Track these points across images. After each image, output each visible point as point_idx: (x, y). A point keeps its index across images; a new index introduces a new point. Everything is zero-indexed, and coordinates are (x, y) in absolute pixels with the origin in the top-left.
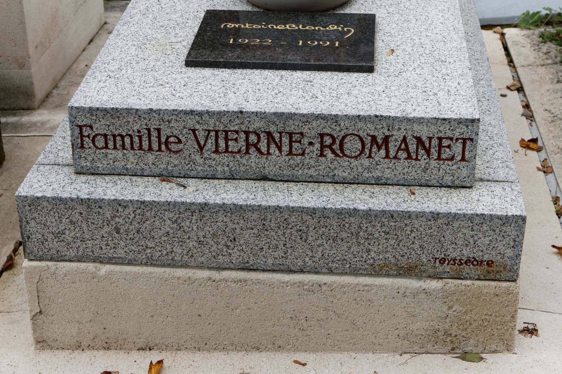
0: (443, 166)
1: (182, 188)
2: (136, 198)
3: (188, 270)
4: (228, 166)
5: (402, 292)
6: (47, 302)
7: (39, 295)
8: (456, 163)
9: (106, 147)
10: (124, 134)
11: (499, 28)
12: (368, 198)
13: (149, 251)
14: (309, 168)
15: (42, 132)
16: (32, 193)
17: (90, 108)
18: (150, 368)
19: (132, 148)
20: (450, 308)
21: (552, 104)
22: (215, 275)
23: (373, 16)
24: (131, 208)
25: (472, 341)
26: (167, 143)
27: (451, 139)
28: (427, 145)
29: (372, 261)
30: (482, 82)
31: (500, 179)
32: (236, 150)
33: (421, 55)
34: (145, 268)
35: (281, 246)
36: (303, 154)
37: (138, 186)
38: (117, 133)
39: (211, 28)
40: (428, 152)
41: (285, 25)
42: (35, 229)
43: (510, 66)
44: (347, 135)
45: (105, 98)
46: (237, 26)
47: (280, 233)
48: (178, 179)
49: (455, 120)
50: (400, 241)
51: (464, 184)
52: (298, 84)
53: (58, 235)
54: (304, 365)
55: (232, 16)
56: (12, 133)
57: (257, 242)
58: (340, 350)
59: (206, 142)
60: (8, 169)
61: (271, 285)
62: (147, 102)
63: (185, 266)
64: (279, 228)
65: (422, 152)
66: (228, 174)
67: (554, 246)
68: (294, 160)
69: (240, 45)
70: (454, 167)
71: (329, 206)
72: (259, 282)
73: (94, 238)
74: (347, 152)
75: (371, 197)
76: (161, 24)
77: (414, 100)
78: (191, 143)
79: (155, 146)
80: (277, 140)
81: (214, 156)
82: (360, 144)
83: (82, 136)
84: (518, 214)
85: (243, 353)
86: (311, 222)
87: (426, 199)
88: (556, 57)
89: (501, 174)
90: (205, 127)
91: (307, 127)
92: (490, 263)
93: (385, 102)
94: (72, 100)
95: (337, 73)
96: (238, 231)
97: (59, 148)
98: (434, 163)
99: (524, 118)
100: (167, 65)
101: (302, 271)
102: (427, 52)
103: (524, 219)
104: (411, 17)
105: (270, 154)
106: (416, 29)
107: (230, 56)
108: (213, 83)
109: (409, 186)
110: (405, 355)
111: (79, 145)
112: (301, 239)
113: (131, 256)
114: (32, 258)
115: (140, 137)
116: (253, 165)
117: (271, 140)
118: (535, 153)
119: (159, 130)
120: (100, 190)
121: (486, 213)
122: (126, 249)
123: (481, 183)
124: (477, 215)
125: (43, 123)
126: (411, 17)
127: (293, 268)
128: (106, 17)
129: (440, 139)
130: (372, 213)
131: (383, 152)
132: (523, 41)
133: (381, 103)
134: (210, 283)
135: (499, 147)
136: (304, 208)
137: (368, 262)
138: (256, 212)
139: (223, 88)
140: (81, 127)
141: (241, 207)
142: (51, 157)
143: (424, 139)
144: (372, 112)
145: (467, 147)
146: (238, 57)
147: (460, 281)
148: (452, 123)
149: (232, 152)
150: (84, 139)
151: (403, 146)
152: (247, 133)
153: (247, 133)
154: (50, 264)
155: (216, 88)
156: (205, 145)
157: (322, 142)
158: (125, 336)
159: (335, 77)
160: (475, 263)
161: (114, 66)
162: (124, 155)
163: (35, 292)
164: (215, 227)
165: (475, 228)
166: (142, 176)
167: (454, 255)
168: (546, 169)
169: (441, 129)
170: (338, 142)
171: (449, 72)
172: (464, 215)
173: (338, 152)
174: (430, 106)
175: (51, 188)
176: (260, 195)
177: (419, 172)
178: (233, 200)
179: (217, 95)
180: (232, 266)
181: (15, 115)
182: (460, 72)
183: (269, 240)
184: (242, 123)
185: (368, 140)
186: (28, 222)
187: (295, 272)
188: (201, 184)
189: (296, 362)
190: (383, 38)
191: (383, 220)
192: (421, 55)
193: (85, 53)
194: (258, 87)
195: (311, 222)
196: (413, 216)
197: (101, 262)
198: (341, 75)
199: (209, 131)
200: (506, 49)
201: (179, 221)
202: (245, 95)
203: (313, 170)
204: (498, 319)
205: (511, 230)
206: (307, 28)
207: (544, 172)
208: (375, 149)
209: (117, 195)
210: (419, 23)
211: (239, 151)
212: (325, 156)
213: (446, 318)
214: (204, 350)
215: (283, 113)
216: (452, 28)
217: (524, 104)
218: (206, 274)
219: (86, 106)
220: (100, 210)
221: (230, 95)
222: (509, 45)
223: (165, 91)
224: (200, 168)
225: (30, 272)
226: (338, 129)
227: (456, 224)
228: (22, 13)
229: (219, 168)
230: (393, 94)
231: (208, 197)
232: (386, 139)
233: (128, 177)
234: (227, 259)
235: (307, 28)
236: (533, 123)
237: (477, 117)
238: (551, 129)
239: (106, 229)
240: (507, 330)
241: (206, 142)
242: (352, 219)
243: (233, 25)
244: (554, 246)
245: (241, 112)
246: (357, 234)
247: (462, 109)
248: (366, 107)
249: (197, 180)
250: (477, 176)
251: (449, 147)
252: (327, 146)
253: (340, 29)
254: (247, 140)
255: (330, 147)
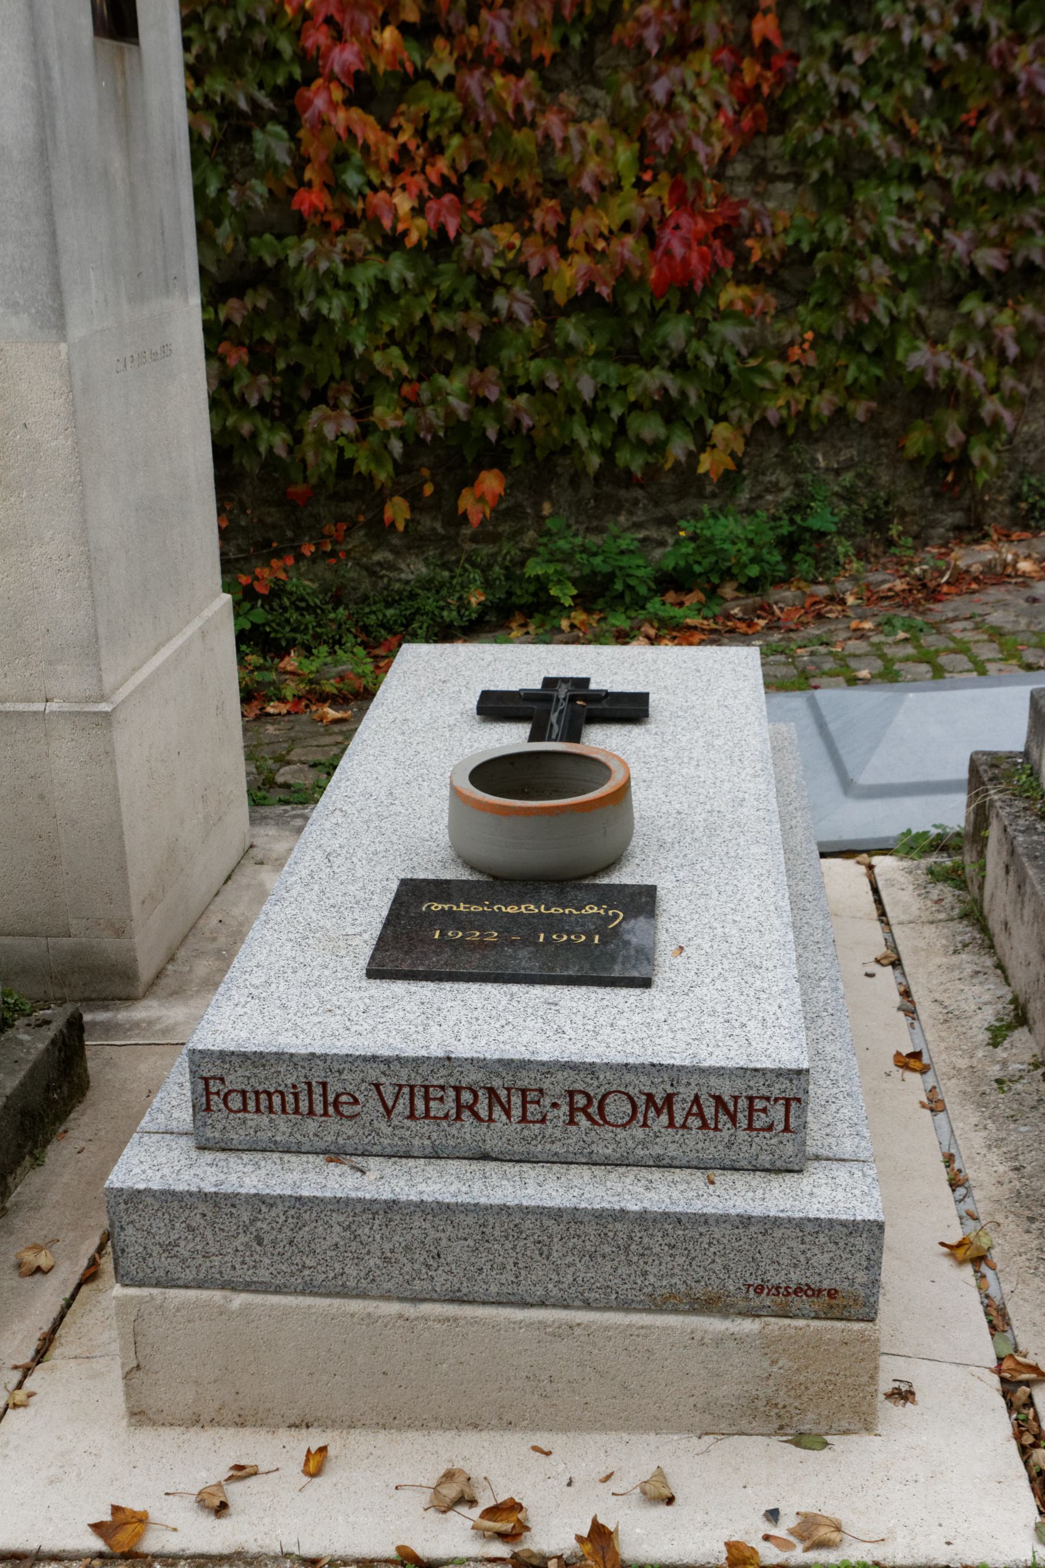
0: (757, 1140)
1: (359, 1174)
2: (288, 1192)
3: (366, 1302)
4: (429, 1138)
5: (698, 1337)
6: (148, 1350)
7: (135, 1339)
8: (776, 1135)
9: (245, 1109)
10: (272, 1090)
11: (865, 855)
12: (642, 1190)
13: (306, 1272)
14: (553, 1142)
15: (148, 1038)
16: (130, 1184)
17: (221, 1052)
18: (307, 1460)
19: (284, 1111)
20: (774, 1362)
21: (945, 991)
22: (410, 1310)
23: (654, 888)
24: (280, 1207)
25: (810, 1416)
26: (336, 1104)
27: (768, 1099)
28: (732, 1108)
29: (650, 1288)
30: (823, 983)
31: (846, 1157)
32: (441, 1114)
33: (724, 956)
34: (301, 1298)
35: (510, 1266)
36: (543, 1121)
37: (291, 1171)
38: (260, 1088)
39: (407, 912)
40: (733, 1118)
41: (519, 904)
42: (134, 1239)
43: (882, 922)
44: (610, 1093)
45: (244, 1035)
46: (446, 907)
47: (508, 1245)
48: (353, 1158)
49: (772, 1071)
50: (693, 1259)
51: (790, 1166)
52: (536, 1008)
53: (169, 1248)
54: (548, 1454)
55: (440, 889)
56: (101, 1039)
57: (473, 1260)
58: (605, 1428)
59: (395, 1102)
60: (93, 1104)
61: (495, 1326)
62: (308, 1041)
63: (363, 1295)
64: (507, 1238)
65: (723, 1118)
66: (430, 1150)
67: (942, 1244)
68: (529, 1129)
69: (451, 942)
70: (774, 1141)
71: (583, 1205)
72: (475, 1321)
73: (224, 1252)
74: (610, 1118)
75: (647, 1189)
76: (332, 901)
77: (710, 1036)
78: (374, 1105)
79: (319, 1108)
80: (504, 1100)
81: (408, 1123)
82: (629, 1106)
83: (208, 1093)
84: (872, 1218)
85: (454, 1432)
86: (556, 1228)
87: (732, 1192)
88: (953, 908)
89: (848, 1147)
90: (395, 1081)
91: (548, 1081)
92: (832, 1293)
93: (667, 1040)
94: (195, 1038)
95: (595, 988)
96: (444, 1243)
97: (174, 1103)
98: (742, 1135)
99: (901, 1014)
100: (339, 975)
101: (542, 1304)
102: (734, 950)
103: (881, 1226)
104: (712, 887)
105: (493, 1121)
106: (718, 910)
107: (435, 962)
108: (408, 1008)
109: (706, 1168)
110: (706, 1438)
111: (204, 1107)
112: (541, 1254)
113: (280, 1280)
114: (127, 1282)
115: (296, 1096)
116: (468, 1136)
117: (494, 1100)
118: (917, 1075)
119: (324, 1085)
120: (233, 1178)
121: (823, 1216)
122: (272, 1269)
123: (816, 1164)
124: (809, 1220)
125: (150, 1023)
126: (712, 887)
127: (529, 1300)
128: (253, 836)
129: (751, 1099)
130: (648, 1216)
131: (664, 1118)
132: (902, 880)
133: (660, 1041)
134: (400, 1322)
135: (836, 1117)
136: (544, 1208)
137: (645, 1290)
138: (471, 1215)
139: (423, 1017)
140: (206, 1080)
141: (448, 1205)
142: (161, 1118)
143: (726, 1098)
144: (647, 1059)
145: (792, 1111)
146: (446, 964)
147: (787, 1321)
148: (768, 1075)
149: (435, 1118)
150: (212, 1097)
151: (695, 1109)
152: (458, 1090)
153: (458, 1090)
154: (155, 1291)
155: (411, 1017)
156: (394, 1107)
157: (571, 1103)
158: (268, 1405)
159: (593, 996)
160: (810, 1292)
161: (258, 978)
162: (271, 1121)
163: (131, 1335)
164: (409, 1237)
165: (807, 1239)
166: (299, 1152)
167: (776, 1281)
168: (935, 1105)
169: (751, 1084)
170: (596, 1103)
171: (766, 985)
172: (790, 1220)
173: (597, 1118)
174: (735, 1046)
175: (159, 1174)
176: (478, 1185)
177: (720, 1148)
178: (437, 1195)
179: (413, 1029)
180: (435, 1296)
181: (106, 1008)
182: (782, 986)
183: (491, 1257)
184: (451, 1075)
185: (641, 1101)
186: (122, 1228)
187: (532, 1305)
188: (388, 1167)
189: (536, 1449)
190: (668, 925)
191: (666, 1226)
192: (724, 956)
193: (218, 899)
194: (476, 1013)
195: (555, 1229)
196: (712, 1221)
197: (233, 1289)
198: (601, 992)
199: (401, 1086)
200: (875, 890)
201: (354, 1227)
202: (456, 1029)
203: (558, 1144)
204: (849, 1381)
205: (861, 1242)
206: (552, 911)
207: (932, 1110)
208: (652, 1114)
209: (260, 1186)
210: (723, 898)
211: (446, 1117)
212: (577, 1124)
213: (768, 1378)
214: (391, 1428)
215: (512, 1061)
216: (772, 908)
217: (902, 989)
218: (392, 1308)
219: (215, 1048)
220: (234, 1210)
221: (433, 1029)
222: (881, 885)
223: (334, 1022)
224: (386, 1142)
225: (123, 1304)
226: (596, 1083)
227: (778, 1233)
228: (123, 852)
229: (416, 1142)
230: (679, 1026)
231: (398, 1190)
232: (669, 1099)
233: (276, 1155)
234: (427, 1285)
235: (552, 911)
236: (916, 1024)
237: (805, 1065)
238: (943, 1034)
239: (242, 1238)
240: (864, 1398)
241: (395, 1102)
242: (618, 1226)
243: (440, 907)
244: (942, 1244)
245: (449, 1059)
246: (627, 1248)
247: (783, 1053)
248: (637, 1049)
249: (382, 1159)
250: (811, 1150)
251: (764, 1110)
252: (579, 1109)
253: (602, 912)
254: (458, 1099)
255: (584, 1110)
